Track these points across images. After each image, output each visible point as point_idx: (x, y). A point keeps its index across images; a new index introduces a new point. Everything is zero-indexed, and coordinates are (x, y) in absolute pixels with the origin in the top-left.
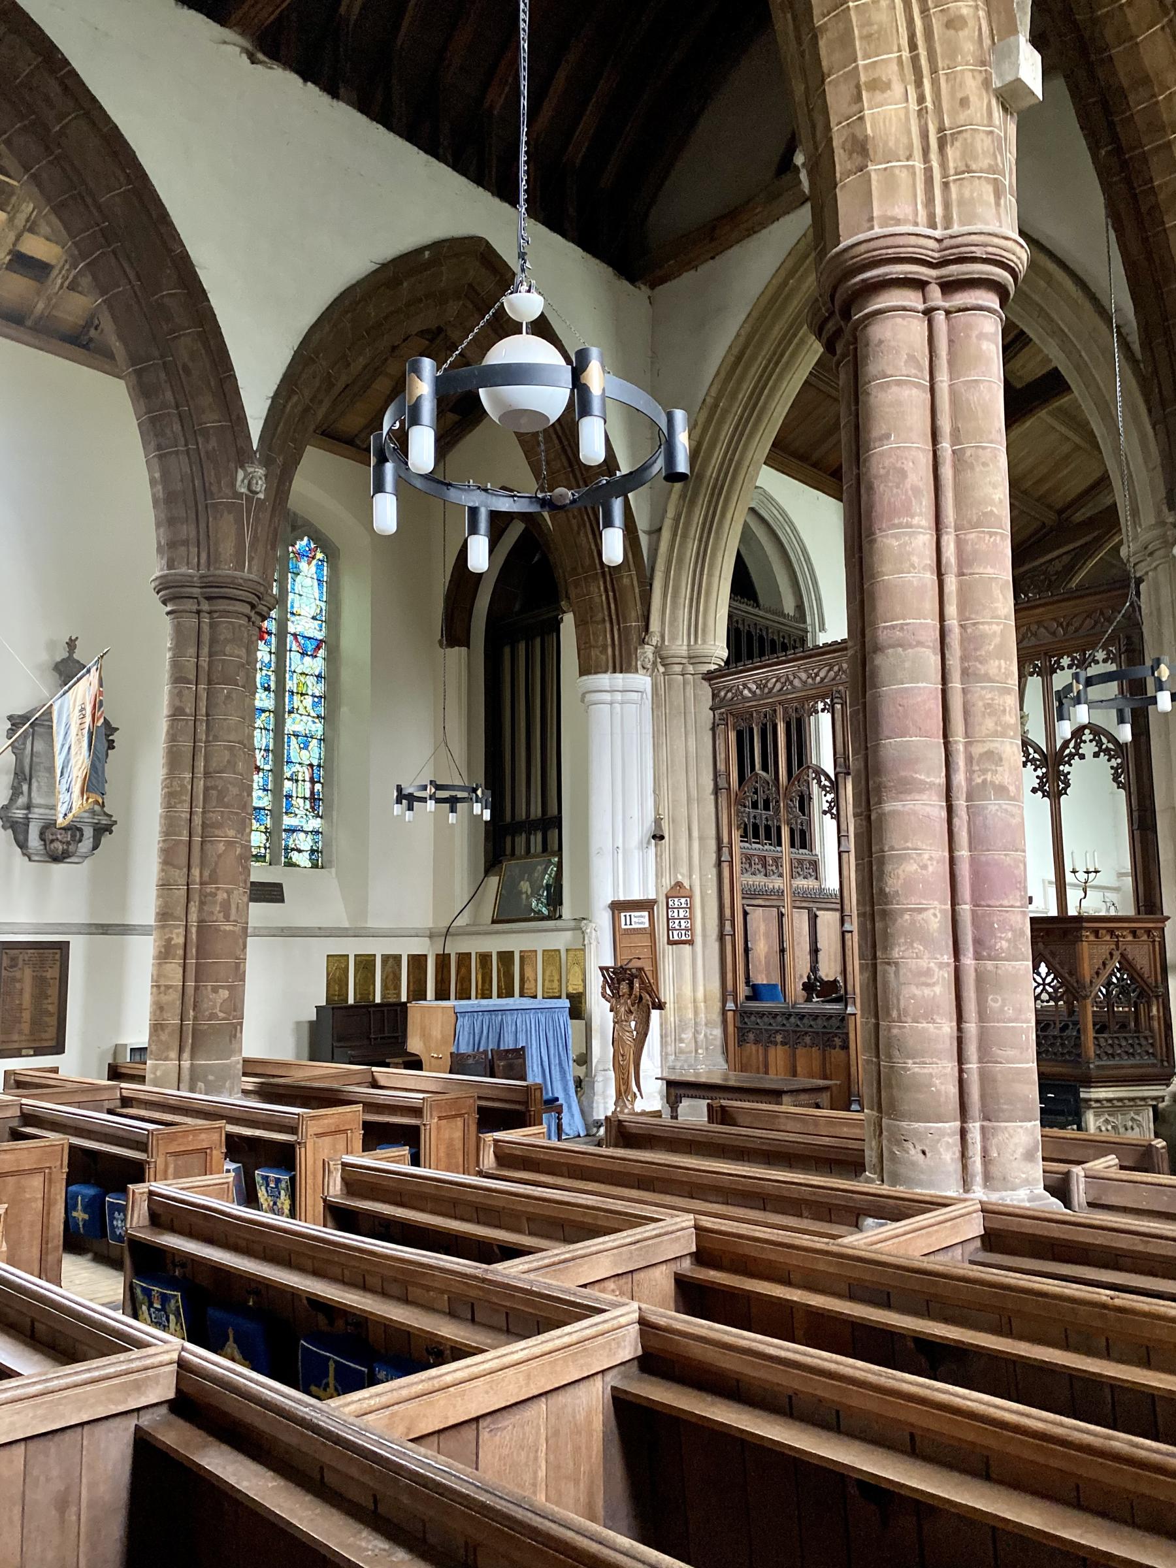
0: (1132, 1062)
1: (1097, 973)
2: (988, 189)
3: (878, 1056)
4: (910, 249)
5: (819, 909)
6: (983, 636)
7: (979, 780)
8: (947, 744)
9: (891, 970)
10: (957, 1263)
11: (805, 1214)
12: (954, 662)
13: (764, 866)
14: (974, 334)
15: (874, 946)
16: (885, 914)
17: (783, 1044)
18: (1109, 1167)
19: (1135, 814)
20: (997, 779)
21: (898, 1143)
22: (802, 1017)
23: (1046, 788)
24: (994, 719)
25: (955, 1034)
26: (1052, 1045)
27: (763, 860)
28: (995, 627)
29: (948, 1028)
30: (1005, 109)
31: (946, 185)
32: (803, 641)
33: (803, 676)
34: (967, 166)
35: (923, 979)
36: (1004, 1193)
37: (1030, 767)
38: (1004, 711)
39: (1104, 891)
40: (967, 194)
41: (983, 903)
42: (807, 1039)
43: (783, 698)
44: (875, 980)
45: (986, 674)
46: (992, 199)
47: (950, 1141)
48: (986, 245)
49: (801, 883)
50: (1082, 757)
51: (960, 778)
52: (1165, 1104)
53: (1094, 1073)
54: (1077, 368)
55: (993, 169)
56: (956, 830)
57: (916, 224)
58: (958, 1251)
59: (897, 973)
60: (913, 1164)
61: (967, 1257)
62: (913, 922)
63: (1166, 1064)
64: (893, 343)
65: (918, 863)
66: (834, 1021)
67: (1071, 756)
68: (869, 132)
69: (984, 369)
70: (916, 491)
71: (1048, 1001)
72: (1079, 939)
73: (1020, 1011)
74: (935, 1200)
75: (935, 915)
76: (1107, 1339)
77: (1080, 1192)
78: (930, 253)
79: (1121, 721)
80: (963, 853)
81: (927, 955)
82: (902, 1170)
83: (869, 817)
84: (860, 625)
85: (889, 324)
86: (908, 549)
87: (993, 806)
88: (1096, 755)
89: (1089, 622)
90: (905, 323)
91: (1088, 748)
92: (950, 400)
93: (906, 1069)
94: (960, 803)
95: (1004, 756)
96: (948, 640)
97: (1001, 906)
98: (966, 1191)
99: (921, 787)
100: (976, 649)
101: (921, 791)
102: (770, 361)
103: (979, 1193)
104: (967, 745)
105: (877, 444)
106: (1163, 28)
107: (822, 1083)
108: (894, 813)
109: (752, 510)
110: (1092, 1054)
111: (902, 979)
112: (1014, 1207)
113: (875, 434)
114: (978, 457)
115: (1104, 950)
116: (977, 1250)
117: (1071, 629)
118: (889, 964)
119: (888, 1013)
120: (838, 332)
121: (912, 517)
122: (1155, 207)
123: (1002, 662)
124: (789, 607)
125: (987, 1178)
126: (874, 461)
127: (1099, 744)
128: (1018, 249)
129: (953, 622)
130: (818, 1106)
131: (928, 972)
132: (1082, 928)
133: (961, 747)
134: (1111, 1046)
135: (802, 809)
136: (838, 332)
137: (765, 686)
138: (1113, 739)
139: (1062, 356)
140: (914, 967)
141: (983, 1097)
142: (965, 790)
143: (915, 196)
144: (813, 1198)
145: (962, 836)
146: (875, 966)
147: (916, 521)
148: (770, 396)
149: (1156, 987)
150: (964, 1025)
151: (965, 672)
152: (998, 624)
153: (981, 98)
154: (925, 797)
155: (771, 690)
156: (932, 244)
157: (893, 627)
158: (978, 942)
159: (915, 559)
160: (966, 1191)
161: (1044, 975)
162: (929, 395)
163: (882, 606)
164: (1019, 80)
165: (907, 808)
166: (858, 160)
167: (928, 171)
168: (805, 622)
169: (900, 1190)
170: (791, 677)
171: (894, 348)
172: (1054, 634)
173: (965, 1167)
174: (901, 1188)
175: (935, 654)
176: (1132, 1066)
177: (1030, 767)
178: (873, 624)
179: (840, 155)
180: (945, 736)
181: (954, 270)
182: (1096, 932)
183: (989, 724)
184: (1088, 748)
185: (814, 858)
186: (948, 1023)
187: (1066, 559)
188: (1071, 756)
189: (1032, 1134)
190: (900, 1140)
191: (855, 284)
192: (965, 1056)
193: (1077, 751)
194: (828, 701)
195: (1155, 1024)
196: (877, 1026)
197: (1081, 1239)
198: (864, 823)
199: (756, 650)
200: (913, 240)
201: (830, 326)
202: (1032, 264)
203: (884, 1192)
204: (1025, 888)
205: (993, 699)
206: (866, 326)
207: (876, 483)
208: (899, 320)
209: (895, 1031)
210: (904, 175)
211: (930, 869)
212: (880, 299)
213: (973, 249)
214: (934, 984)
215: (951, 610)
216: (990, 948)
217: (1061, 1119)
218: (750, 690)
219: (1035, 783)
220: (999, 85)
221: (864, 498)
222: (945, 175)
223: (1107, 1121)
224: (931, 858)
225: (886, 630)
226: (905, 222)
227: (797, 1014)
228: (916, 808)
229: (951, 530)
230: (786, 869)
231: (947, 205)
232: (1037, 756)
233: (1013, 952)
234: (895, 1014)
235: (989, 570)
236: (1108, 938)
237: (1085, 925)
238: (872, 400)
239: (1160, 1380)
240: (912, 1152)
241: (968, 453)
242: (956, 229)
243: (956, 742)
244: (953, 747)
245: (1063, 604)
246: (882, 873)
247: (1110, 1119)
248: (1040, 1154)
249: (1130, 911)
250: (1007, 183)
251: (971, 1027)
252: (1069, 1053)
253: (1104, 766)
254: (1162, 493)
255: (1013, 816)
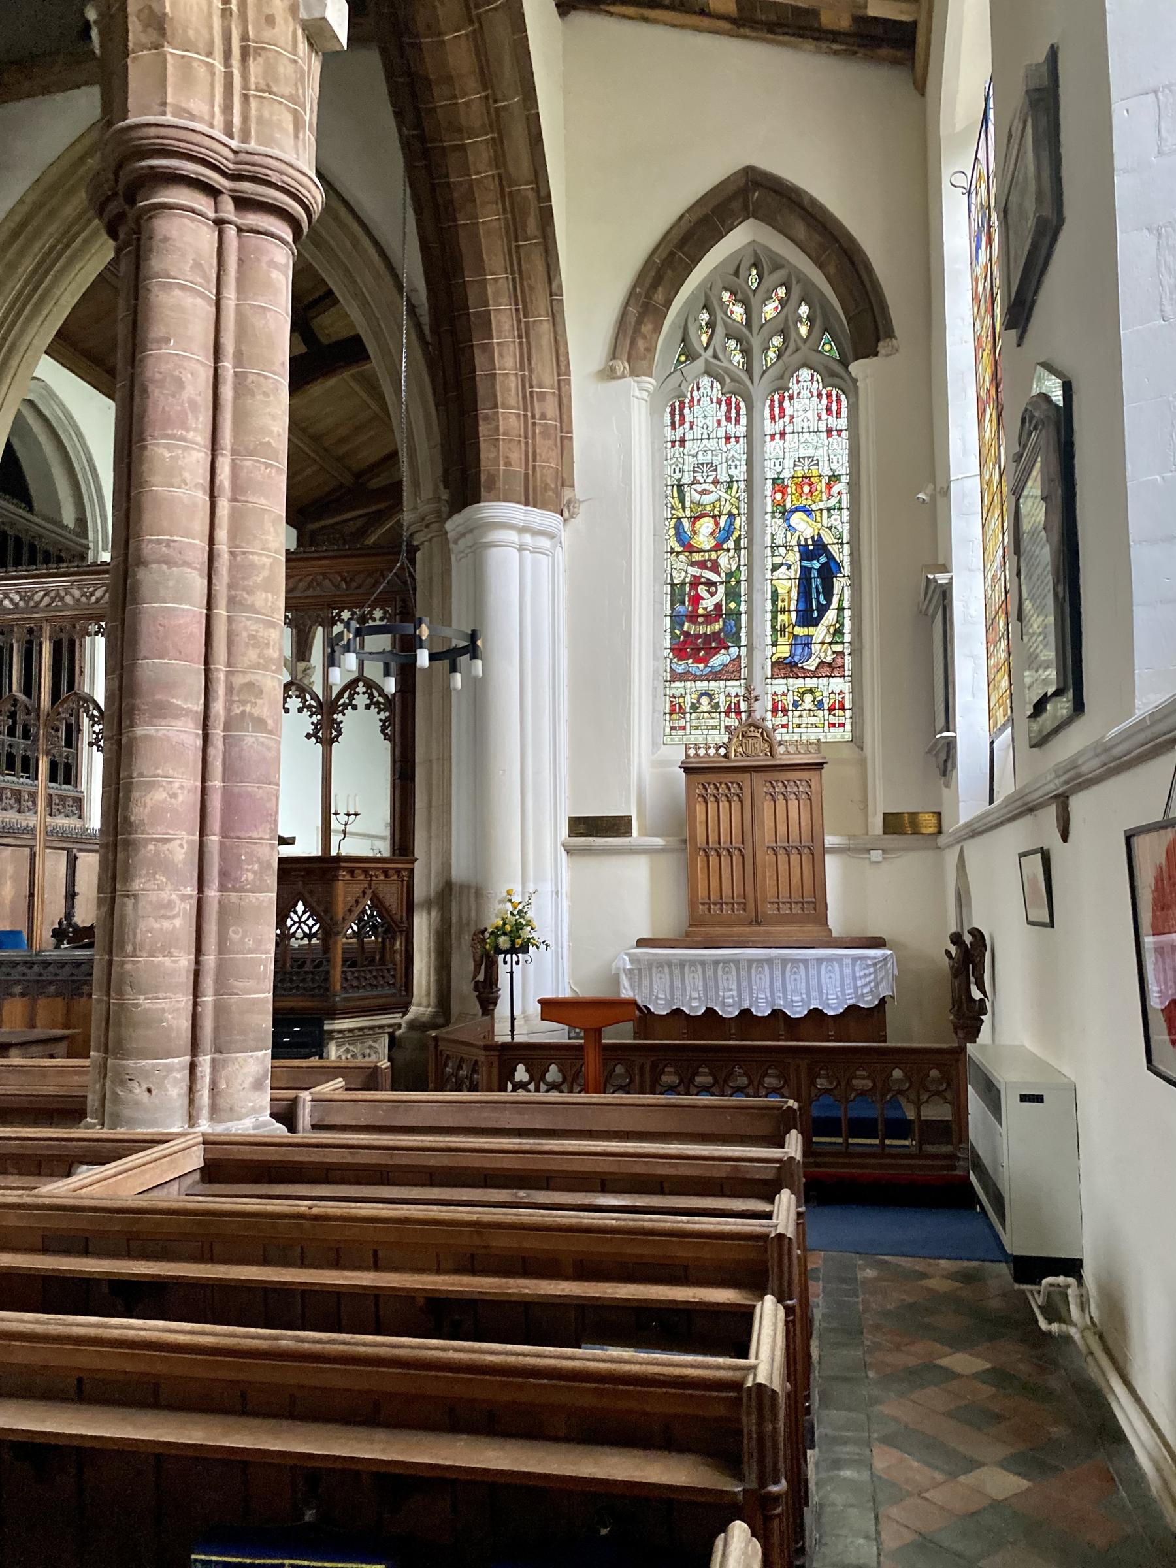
0: (375, 993)
1: (350, 911)
2: (288, 119)
3: (109, 995)
4: (203, 150)
5: (80, 850)
6: (252, 565)
7: (238, 711)
8: (207, 671)
9: (130, 902)
10: (173, 1198)
11: (11, 1170)
12: (221, 587)
13: (18, 801)
14: (265, 259)
15: (114, 878)
16: (128, 843)
17: (22, 995)
18: (336, 1089)
19: (398, 765)
20: (256, 712)
21: (122, 1083)
22: (46, 964)
23: (320, 734)
24: (258, 651)
25: (193, 966)
26: (304, 980)
27: (17, 796)
28: (264, 559)
29: (184, 961)
30: (310, 44)
31: (246, 98)
32: (83, 557)
33: (77, 593)
34: (268, 85)
35: (162, 912)
36: (229, 1124)
37: (306, 713)
38: (268, 645)
39: (365, 834)
40: (266, 114)
41: (232, 835)
42: (52, 988)
43: (52, 614)
44: (112, 914)
45: (253, 605)
46: (291, 128)
47: (178, 1076)
48: (282, 173)
49: (61, 821)
50: (355, 708)
51: (218, 707)
52: (401, 1031)
53: (339, 1006)
54: (375, 333)
55: (293, 99)
56: (210, 759)
57: (212, 126)
58: (175, 1186)
59: (135, 906)
60: (137, 1103)
61: (183, 1191)
62: (157, 853)
63: (404, 993)
64: (178, 245)
65: (169, 792)
66: (84, 968)
67: (345, 706)
68: (168, 10)
69: (272, 298)
70: (193, 404)
71: (302, 939)
72: (335, 878)
73: (259, 942)
74: (155, 1137)
75: (181, 846)
76: (302, 1248)
77: (305, 1117)
78: (225, 161)
79: (387, 673)
80: (216, 783)
81: (169, 887)
82: (126, 1112)
83: (119, 742)
84: (124, 535)
85: (177, 221)
86: (180, 465)
87: (250, 738)
88: (368, 707)
89: (370, 581)
90: (193, 226)
91: (361, 700)
92: (236, 320)
93: (136, 1006)
94: (217, 733)
95: (264, 689)
96: (216, 564)
97: (250, 838)
98: (191, 1126)
99: (179, 712)
100: (243, 578)
101: (177, 717)
102: (58, 241)
103: (205, 1126)
104: (228, 674)
105: (154, 346)
106: (466, 35)
107: (58, 1032)
108: (147, 737)
109: (30, 403)
110: (338, 987)
111: (140, 913)
112: (235, 1135)
113: (152, 335)
114: (259, 385)
115: (357, 889)
116: (195, 1183)
117: (354, 585)
118: (128, 896)
119: (122, 948)
120: (121, 217)
121: (188, 430)
122: (451, 201)
123: (269, 595)
124: (68, 517)
125: (214, 1110)
126: (150, 362)
127: (371, 696)
128: (313, 188)
129: (222, 547)
130: (52, 1057)
131: (170, 905)
132: (340, 868)
133: (222, 676)
134: (357, 978)
135: (69, 744)
136: (121, 217)
137: (31, 598)
138: (381, 692)
139: (365, 324)
140: (154, 899)
141: (216, 1029)
142: (223, 719)
143: (213, 96)
144: (22, 1151)
145: (217, 765)
146: (113, 899)
147: (190, 435)
148: (57, 279)
149: (402, 922)
150: (202, 958)
151: (232, 601)
152: (268, 556)
153: (286, 21)
154: (180, 723)
155: (37, 604)
156: (231, 156)
157: (159, 542)
158: (224, 874)
159: (186, 475)
160: (191, 1126)
161: (300, 913)
162: (214, 309)
163: (148, 518)
164: (324, 19)
165: (160, 734)
166: (154, 36)
167: (229, 76)
168: (86, 538)
169: (121, 1132)
170: (62, 593)
171: (179, 249)
172: (337, 587)
173: (191, 1101)
174: (122, 1130)
175: (202, 577)
176: (375, 997)
177: (306, 713)
178: (138, 535)
179: (134, 25)
180: (207, 662)
181: (248, 187)
182: (351, 872)
183: (252, 655)
184: (361, 700)
185: (80, 795)
186: (186, 957)
187: (359, 523)
188: (345, 706)
189: (263, 1062)
190: (124, 1080)
191: (142, 168)
192: (201, 989)
193: (351, 701)
194: (103, 624)
195: (398, 957)
196: (110, 962)
197: (296, 1159)
198: (115, 747)
199: (25, 557)
200: (207, 142)
201: (113, 208)
202: (327, 207)
203: (104, 1136)
204: (276, 822)
205: (257, 631)
206: (151, 217)
207: (151, 387)
208: (187, 221)
209: (128, 967)
210: (202, 71)
211: (181, 798)
212: (167, 192)
213: (269, 172)
214: (174, 917)
215: (222, 535)
216: (237, 880)
217: (303, 1051)
218: (11, 600)
219: (310, 729)
220: (306, 17)
221: (137, 399)
222: (245, 85)
223: (347, 1051)
224: (182, 787)
225: (151, 543)
226: (201, 120)
227: (43, 962)
228: (170, 734)
229: (227, 453)
230: (41, 801)
231: (245, 119)
232: (313, 703)
233: (258, 883)
234: (129, 948)
235: (263, 501)
236: (362, 878)
237: (343, 865)
238: (152, 297)
239: (346, 1278)
240: (137, 1091)
241: (251, 378)
242: (253, 145)
243: (217, 669)
244: (214, 675)
245: (347, 560)
246: (128, 798)
247: (351, 1048)
248: (269, 1081)
249: (387, 853)
250: (307, 118)
251: (210, 960)
252: (319, 987)
253: (374, 718)
254: (439, 472)
255: (269, 749)
